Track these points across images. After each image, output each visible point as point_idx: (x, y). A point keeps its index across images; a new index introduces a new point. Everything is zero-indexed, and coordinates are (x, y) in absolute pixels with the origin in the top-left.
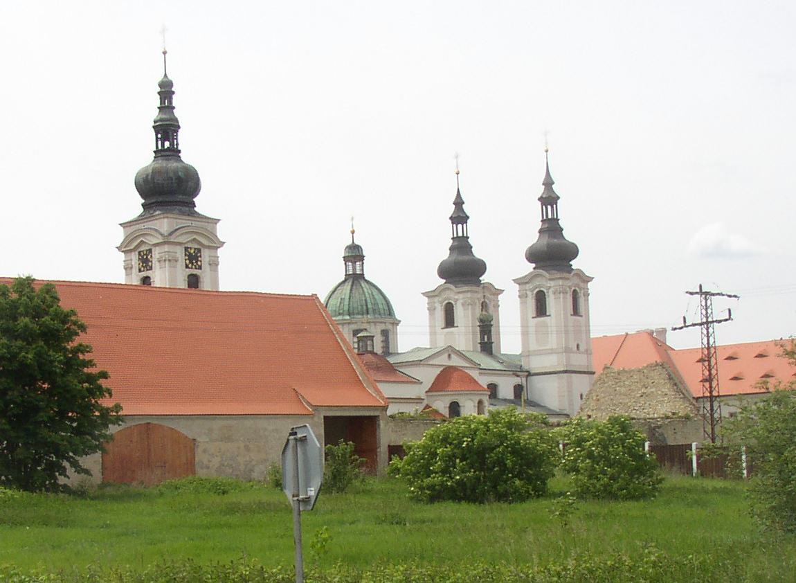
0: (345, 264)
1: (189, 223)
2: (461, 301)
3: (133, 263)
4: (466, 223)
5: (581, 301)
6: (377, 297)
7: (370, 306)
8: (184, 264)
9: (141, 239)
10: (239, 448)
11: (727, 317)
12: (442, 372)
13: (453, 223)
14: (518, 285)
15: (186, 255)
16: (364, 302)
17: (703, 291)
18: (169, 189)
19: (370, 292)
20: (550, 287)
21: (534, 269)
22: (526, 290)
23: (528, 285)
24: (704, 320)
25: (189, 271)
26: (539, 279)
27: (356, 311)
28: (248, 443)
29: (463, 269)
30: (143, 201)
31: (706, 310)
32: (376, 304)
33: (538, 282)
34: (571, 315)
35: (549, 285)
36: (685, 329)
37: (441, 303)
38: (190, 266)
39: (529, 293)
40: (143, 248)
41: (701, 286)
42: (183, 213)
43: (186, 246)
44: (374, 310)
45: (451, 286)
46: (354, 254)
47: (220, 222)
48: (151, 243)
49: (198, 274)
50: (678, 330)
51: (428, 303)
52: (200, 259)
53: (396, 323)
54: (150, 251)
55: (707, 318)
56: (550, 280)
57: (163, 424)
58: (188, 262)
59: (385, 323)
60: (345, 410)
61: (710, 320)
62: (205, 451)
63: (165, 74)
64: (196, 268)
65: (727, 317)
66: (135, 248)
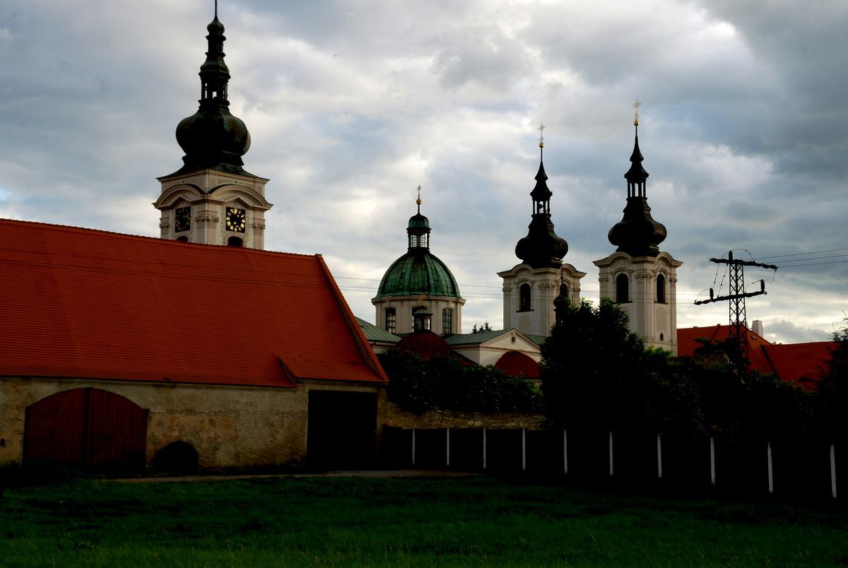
0: (409, 236)
1: (233, 181)
2: (539, 283)
3: (170, 222)
4: (549, 200)
5: (668, 286)
6: (440, 273)
7: (432, 282)
8: (225, 226)
9: (180, 195)
10: (202, 422)
11: (760, 290)
12: (504, 356)
13: (534, 200)
14: (598, 268)
15: (227, 216)
16: (426, 277)
17: (734, 259)
18: (213, 139)
19: (433, 268)
20: (633, 271)
21: (617, 250)
22: (607, 273)
23: (610, 268)
24: (734, 293)
25: (230, 234)
26: (622, 262)
27: (416, 287)
28: (214, 417)
29: (541, 246)
30: (185, 154)
31: (736, 281)
32: (438, 280)
33: (620, 264)
34: (655, 302)
35: (632, 269)
36: (711, 303)
37: (517, 284)
38: (232, 228)
39: (610, 277)
40: (182, 206)
41: (731, 254)
42: (225, 170)
43: (228, 206)
44: (436, 287)
45: (530, 268)
46: (418, 226)
47: (269, 182)
48: (190, 201)
49: (241, 237)
50: (703, 301)
51: (503, 284)
52: (243, 221)
53: (459, 301)
54: (188, 209)
55: (737, 291)
56: (634, 263)
57: (95, 387)
58: (229, 223)
59: (448, 301)
60: (334, 384)
61: (740, 293)
62: (160, 424)
63: (542, 163)
64: (238, 231)
65: (760, 290)
66: (172, 205)
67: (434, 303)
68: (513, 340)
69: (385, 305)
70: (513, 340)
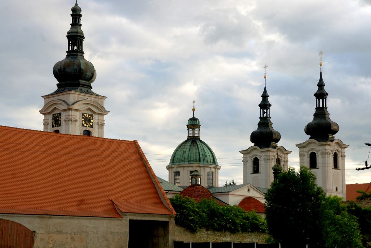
58: (84, 122)
67: (202, 169)
68: (249, 190)
69: (175, 170)
70: (249, 190)
